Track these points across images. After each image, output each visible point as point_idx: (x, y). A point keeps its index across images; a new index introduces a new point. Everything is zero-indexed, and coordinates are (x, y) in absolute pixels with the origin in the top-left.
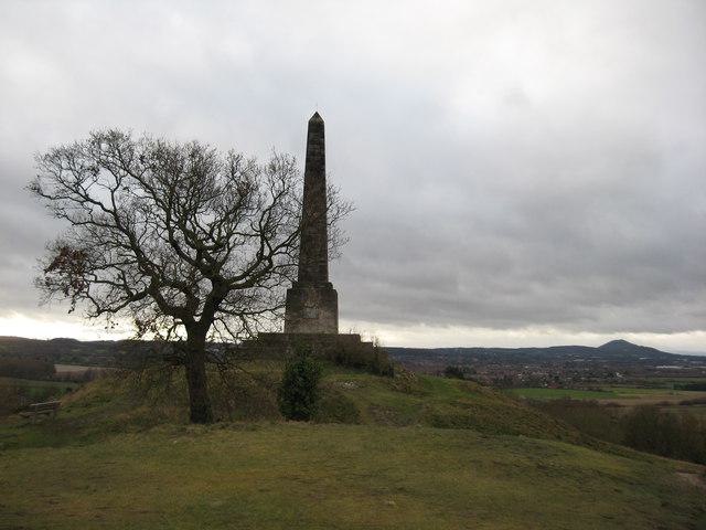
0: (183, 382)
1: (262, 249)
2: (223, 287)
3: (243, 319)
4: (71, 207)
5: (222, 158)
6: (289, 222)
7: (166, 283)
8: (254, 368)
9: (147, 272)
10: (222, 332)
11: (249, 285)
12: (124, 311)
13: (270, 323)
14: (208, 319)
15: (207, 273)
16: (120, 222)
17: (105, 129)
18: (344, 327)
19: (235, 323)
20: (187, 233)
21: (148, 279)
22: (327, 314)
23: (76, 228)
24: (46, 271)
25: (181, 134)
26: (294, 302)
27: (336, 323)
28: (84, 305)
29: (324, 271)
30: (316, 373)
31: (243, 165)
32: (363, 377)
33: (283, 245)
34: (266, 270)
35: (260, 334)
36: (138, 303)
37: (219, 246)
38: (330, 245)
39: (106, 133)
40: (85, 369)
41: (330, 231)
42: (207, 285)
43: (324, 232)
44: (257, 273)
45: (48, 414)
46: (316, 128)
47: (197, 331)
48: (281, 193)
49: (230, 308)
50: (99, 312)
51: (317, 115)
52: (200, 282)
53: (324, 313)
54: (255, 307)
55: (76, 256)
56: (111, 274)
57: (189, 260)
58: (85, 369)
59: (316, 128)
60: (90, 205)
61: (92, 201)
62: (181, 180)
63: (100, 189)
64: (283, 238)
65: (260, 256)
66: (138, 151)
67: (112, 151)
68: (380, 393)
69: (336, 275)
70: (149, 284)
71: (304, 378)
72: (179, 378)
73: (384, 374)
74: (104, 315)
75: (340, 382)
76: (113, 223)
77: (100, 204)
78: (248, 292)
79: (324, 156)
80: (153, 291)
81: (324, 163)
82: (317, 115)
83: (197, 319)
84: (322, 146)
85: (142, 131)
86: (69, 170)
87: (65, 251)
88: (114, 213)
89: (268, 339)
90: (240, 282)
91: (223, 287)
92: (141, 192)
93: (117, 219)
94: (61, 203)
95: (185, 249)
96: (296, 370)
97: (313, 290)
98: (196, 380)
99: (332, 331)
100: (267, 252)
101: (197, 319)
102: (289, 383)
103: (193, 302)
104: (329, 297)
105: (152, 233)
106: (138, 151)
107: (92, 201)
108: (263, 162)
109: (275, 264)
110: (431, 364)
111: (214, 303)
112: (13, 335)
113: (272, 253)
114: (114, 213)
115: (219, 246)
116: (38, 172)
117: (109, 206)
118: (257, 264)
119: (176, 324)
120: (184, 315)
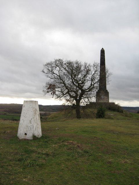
0: (75, 111)
1: (92, 83)
2: (83, 92)
3: (88, 98)
4: (50, 75)
5: (83, 64)
6: (97, 78)
7: (71, 91)
8: (91, 110)
9: (67, 88)
10: (84, 102)
11: (89, 91)
12: (62, 97)
13: (94, 100)
14: (80, 99)
15: (80, 89)
16: (60, 78)
17: (58, 58)
18: (111, 101)
19: (86, 100)
20: (75, 80)
21: (67, 90)
22: (106, 98)
23: (51, 79)
24: (47, 89)
25: (73, 57)
26: (98, 95)
27: (109, 100)
28: (55, 96)
29: (105, 87)
30: (104, 109)
31: (88, 65)
32: (115, 113)
33: (96, 82)
34: (93, 88)
35: (90, 103)
36: (65, 95)
37: (83, 83)
38: (107, 82)
39: (58, 59)
40: (44, 112)
41: (107, 79)
42: (80, 91)
43: (105, 79)
44: (90, 89)
45: (45, 120)
46: (103, 52)
47: (78, 102)
48: (95, 72)
49: (85, 96)
50: (58, 97)
51: (103, 48)
52: (76, 90)
53: (105, 97)
54: (91, 96)
55: (53, 86)
56: (59, 89)
57: (76, 86)
58: (44, 112)
59: (103, 52)
60: (54, 74)
61: (55, 74)
62: (73, 69)
63: (56, 71)
64: (97, 81)
65: (91, 84)
66: (64, 63)
67: (59, 63)
68: (119, 116)
69: (108, 87)
70: (68, 91)
71: (102, 111)
72: (74, 112)
73: (121, 112)
74: (59, 98)
75: (109, 113)
76: (59, 78)
77: (56, 74)
78: (89, 93)
79: (105, 59)
80: (68, 93)
81: (105, 61)
82: (103, 48)
83: (78, 99)
84: (104, 56)
85: (65, 60)
86: (50, 67)
87: (50, 85)
88: (59, 76)
89: (92, 104)
90: (87, 90)
91: (83, 92)
92: (64, 71)
93: (60, 77)
94: (48, 74)
95: (75, 83)
96: (100, 110)
97: (103, 91)
98: (78, 112)
99: (108, 102)
100: (93, 84)
101: (78, 99)
102: (98, 113)
103: (77, 95)
104: (107, 93)
105: (68, 82)
106: (64, 63)
107: (55, 74)
108: (92, 64)
109: (95, 86)
110: (135, 111)
111: (81, 95)
112: (15, 103)
113: (94, 84)
114: (59, 76)
115: (83, 83)
116: (44, 68)
117: (58, 75)
118: (91, 86)
119: (74, 100)
120: (75, 98)
